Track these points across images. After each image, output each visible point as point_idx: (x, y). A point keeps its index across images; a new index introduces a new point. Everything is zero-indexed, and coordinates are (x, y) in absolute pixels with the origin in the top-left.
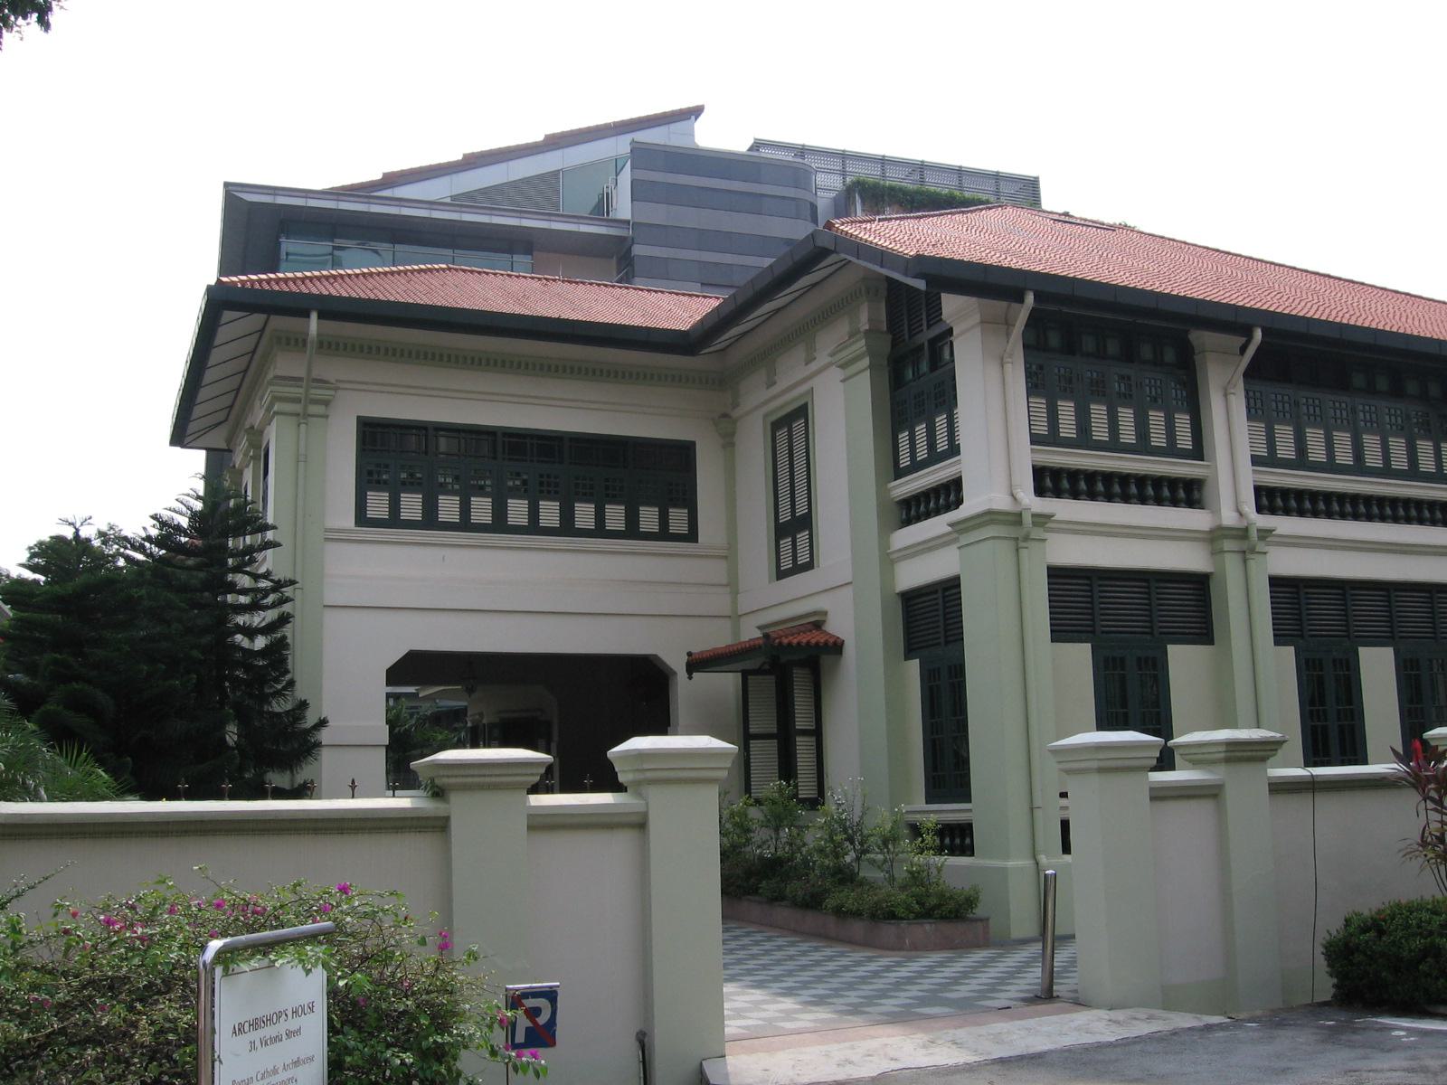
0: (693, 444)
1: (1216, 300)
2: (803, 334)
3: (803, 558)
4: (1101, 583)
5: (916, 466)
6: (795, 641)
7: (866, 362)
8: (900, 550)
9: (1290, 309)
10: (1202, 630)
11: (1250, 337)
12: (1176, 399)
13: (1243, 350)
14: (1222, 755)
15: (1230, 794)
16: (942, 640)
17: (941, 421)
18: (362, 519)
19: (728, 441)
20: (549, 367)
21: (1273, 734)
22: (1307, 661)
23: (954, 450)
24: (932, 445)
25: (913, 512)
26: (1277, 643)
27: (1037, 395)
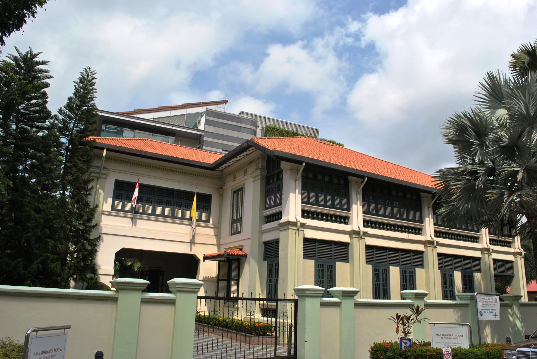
0: (212, 195)
1: (353, 168)
2: (244, 168)
3: (238, 230)
4: (318, 245)
5: (271, 207)
6: (233, 253)
7: (260, 177)
8: (264, 230)
9: (378, 173)
10: (345, 259)
11: (364, 179)
12: (395, 204)
13: (362, 182)
14: (469, 298)
15: (343, 304)
16: (274, 256)
17: (278, 195)
18: (113, 208)
19: (221, 196)
20: (139, 164)
21: (358, 290)
22: (318, 265)
23: (281, 204)
24: (275, 202)
25: (269, 220)
26: (366, 264)
27: (305, 190)
